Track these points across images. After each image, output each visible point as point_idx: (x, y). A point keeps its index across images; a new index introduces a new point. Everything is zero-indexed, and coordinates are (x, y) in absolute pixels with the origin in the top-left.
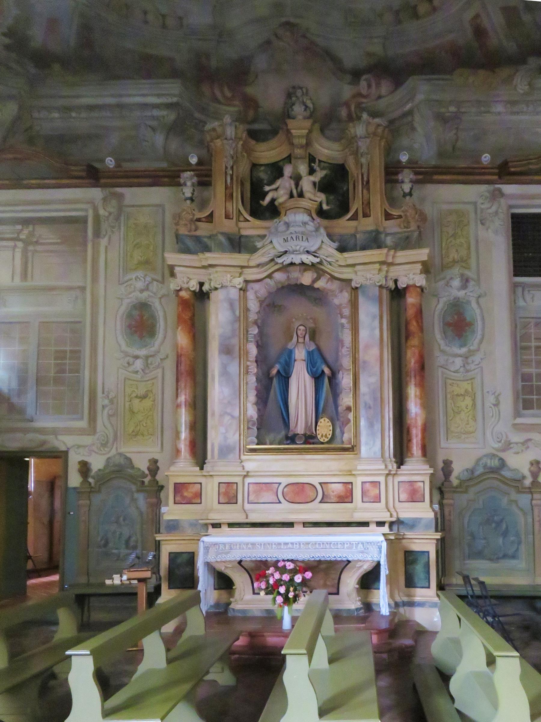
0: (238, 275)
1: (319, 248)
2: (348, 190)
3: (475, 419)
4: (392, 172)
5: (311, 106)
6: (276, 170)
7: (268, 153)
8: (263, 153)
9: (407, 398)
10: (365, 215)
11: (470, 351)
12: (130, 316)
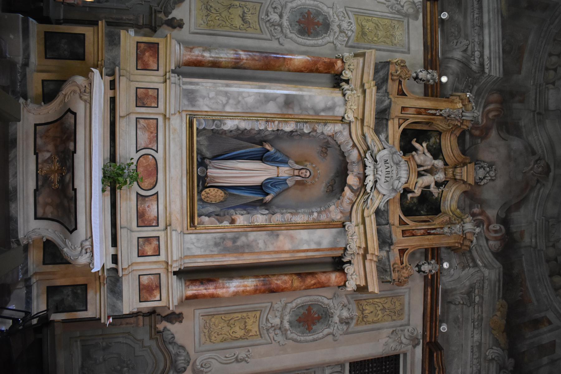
0: (356, 116)
1: (379, 192)
2: (421, 215)
3: (224, 340)
4: (433, 254)
5: (482, 183)
6: (436, 153)
7: (449, 145)
8: (449, 142)
9: (242, 277)
10: (404, 232)
11: (286, 330)
12: (319, 13)
